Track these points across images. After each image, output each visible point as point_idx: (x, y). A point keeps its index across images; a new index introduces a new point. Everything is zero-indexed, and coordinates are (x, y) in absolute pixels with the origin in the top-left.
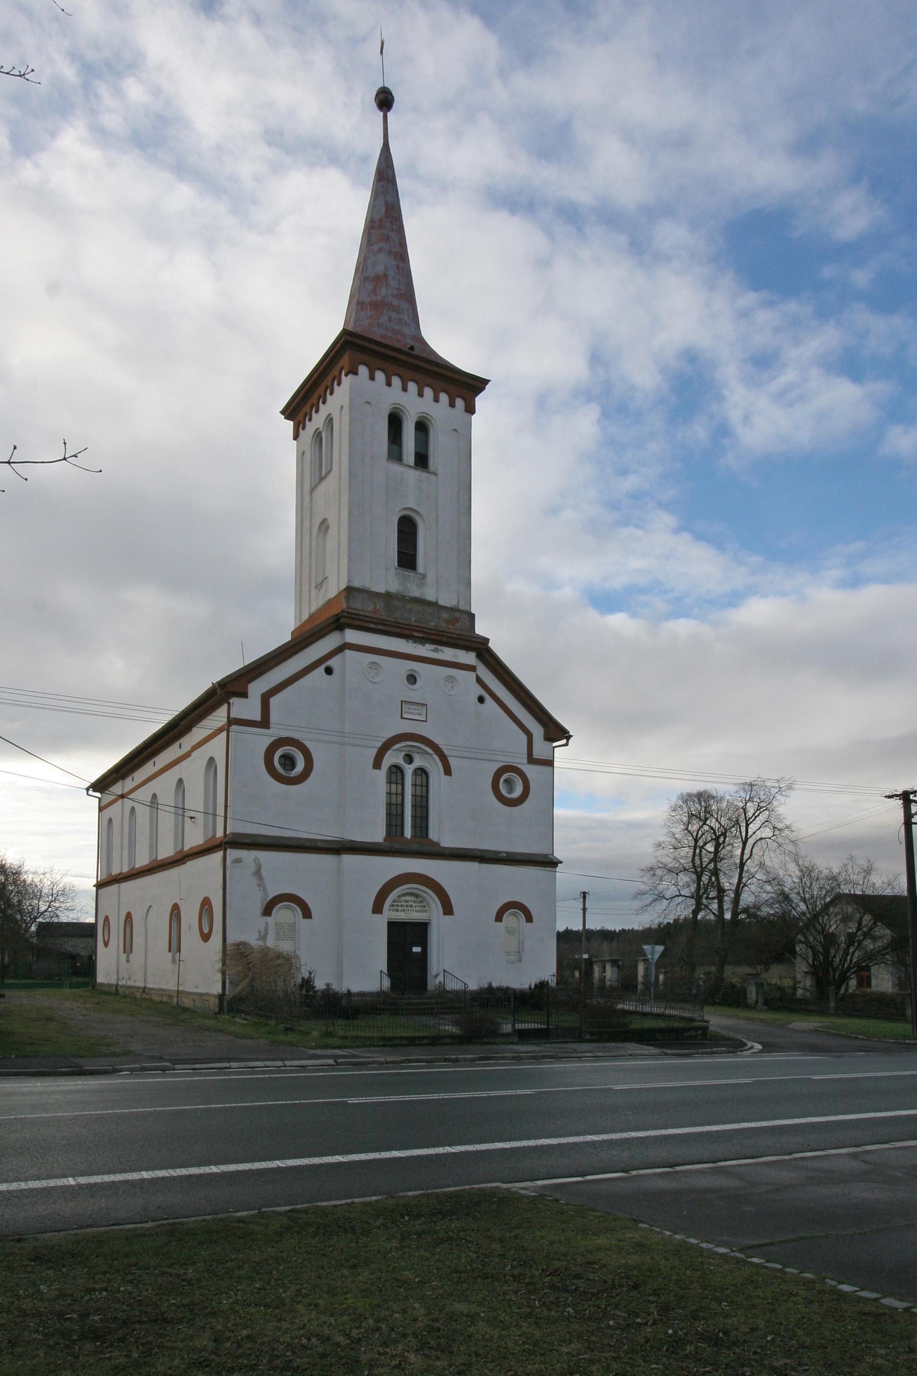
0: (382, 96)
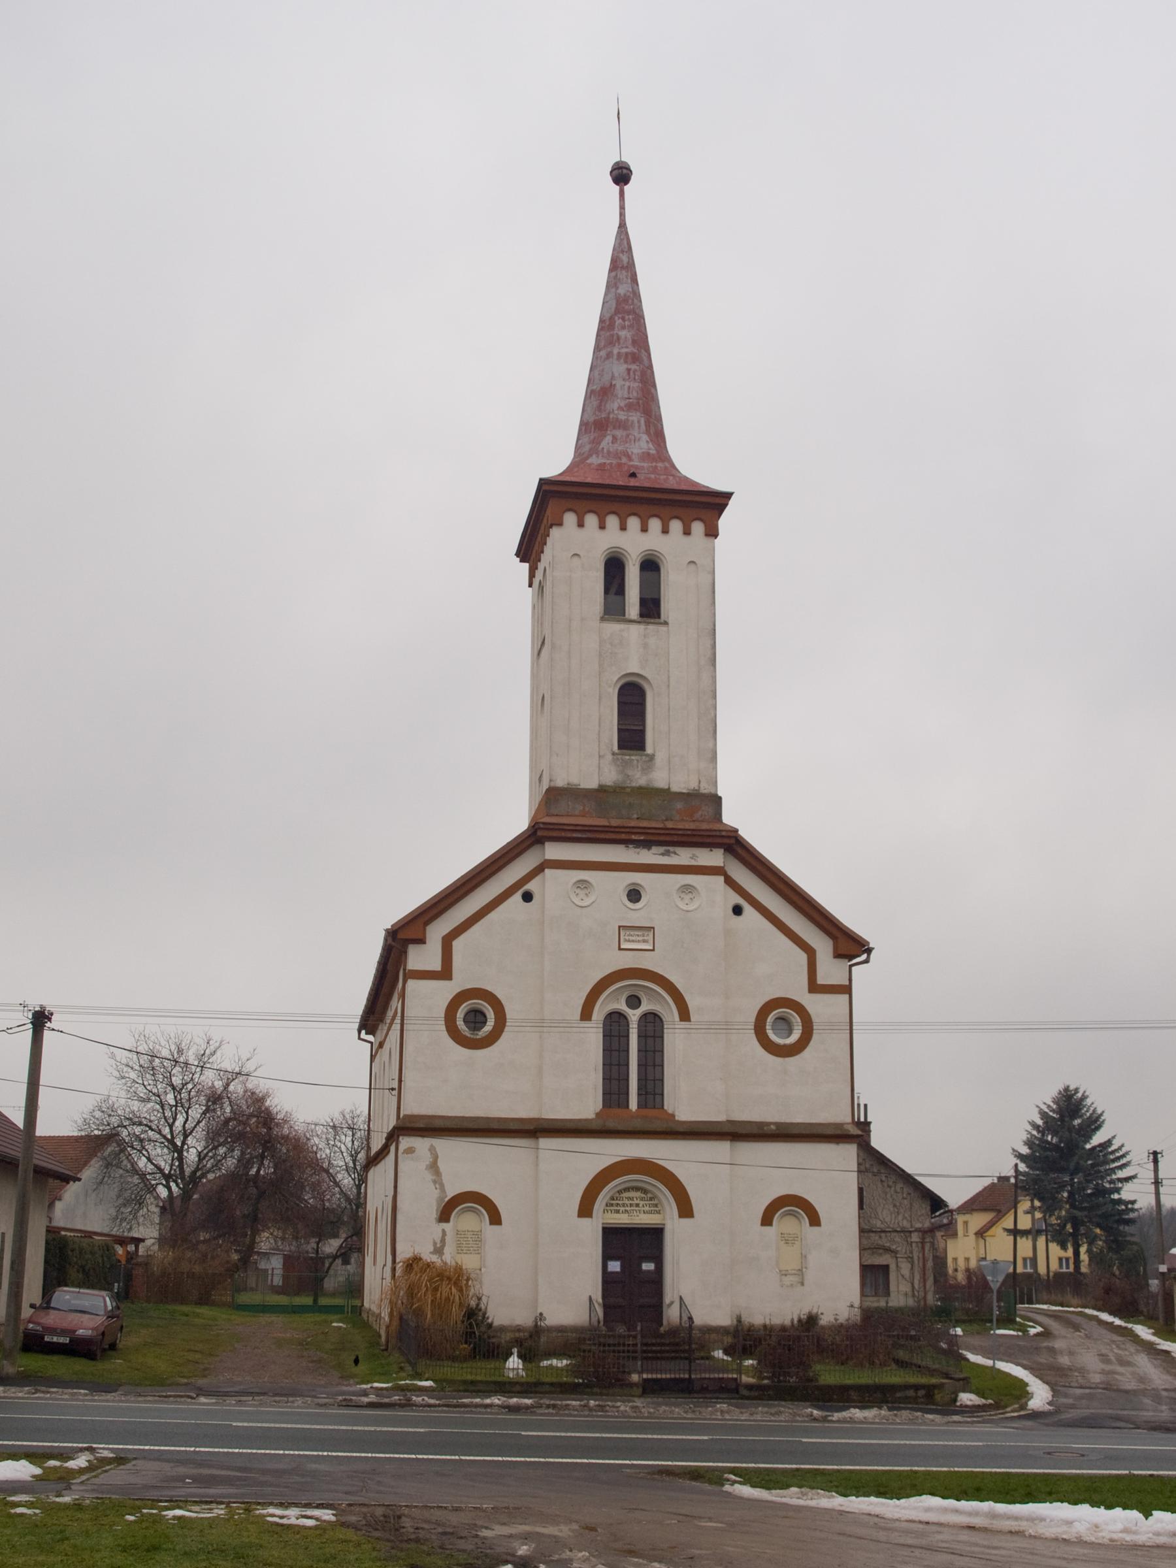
0: (616, 172)
